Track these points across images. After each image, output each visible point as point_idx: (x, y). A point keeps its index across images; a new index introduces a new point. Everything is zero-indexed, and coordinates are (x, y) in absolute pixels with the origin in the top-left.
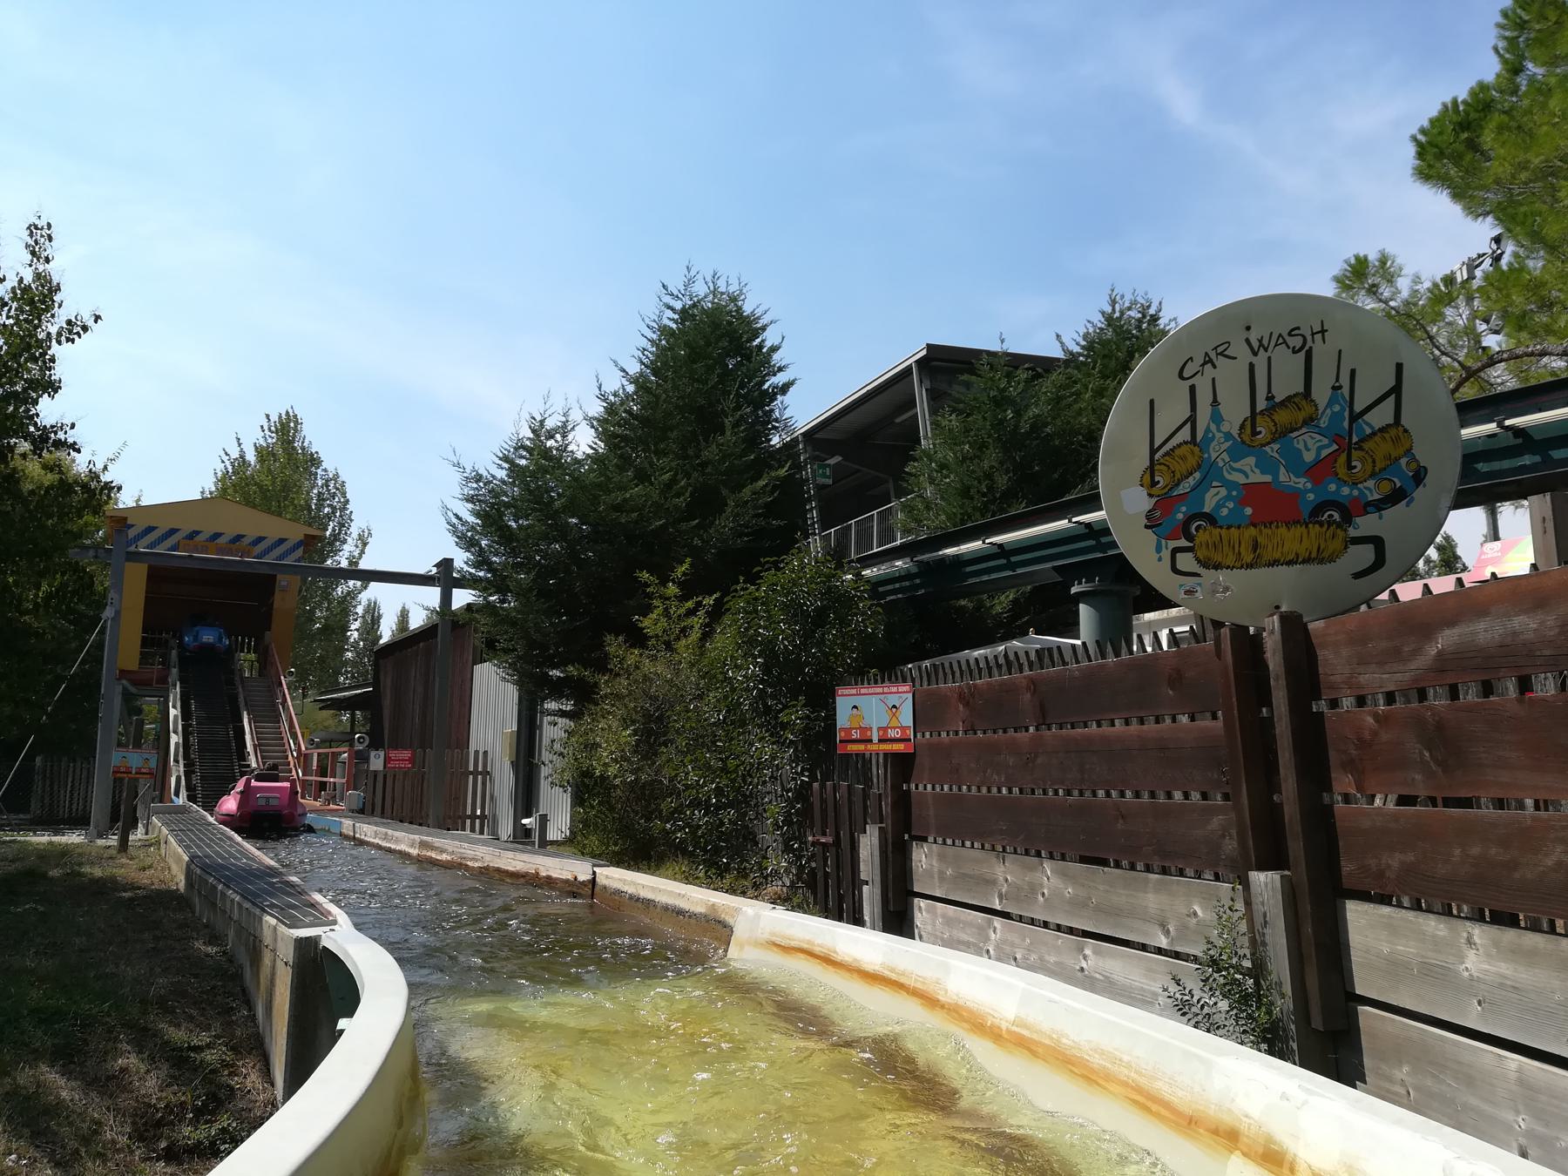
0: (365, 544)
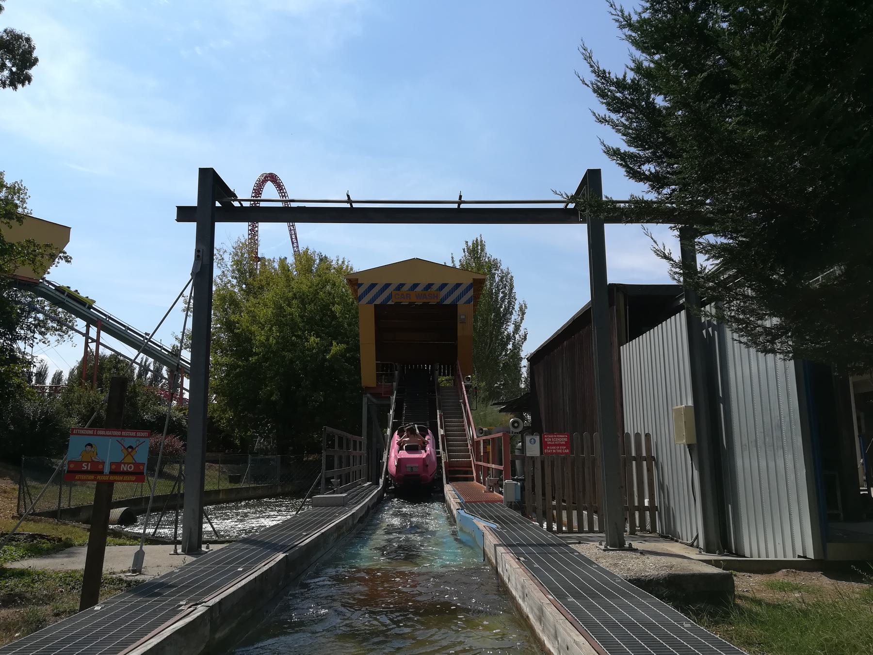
0: (523, 314)
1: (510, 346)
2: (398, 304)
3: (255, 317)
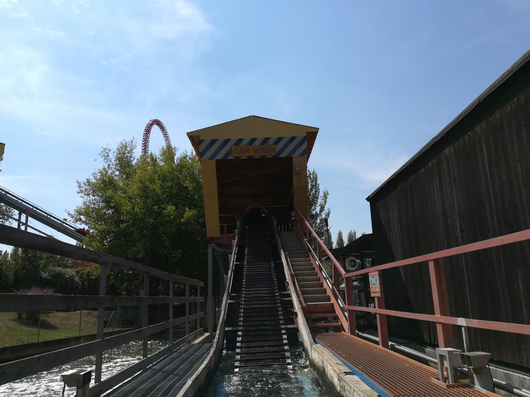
0: (326, 198)
1: (318, 221)
2: (237, 158)
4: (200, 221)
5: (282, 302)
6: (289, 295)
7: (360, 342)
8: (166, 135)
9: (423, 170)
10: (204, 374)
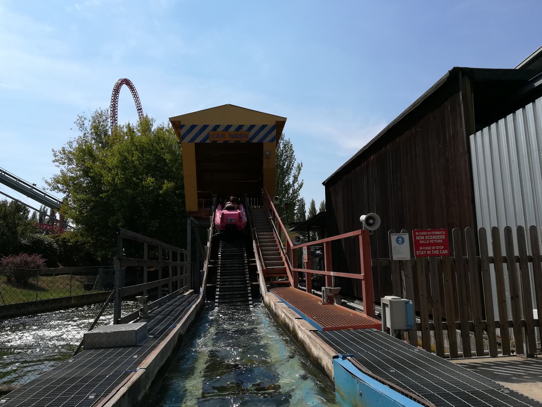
0: (300, 169)
1: (291, 191)
2: (214, 142)
3: (104, 163)
4: (179, 192)
5: (249, 266)
6: (255, 262)
7: (350, 313)
8: (135, 95)
9: (358, 168)
10: (177, 338)
